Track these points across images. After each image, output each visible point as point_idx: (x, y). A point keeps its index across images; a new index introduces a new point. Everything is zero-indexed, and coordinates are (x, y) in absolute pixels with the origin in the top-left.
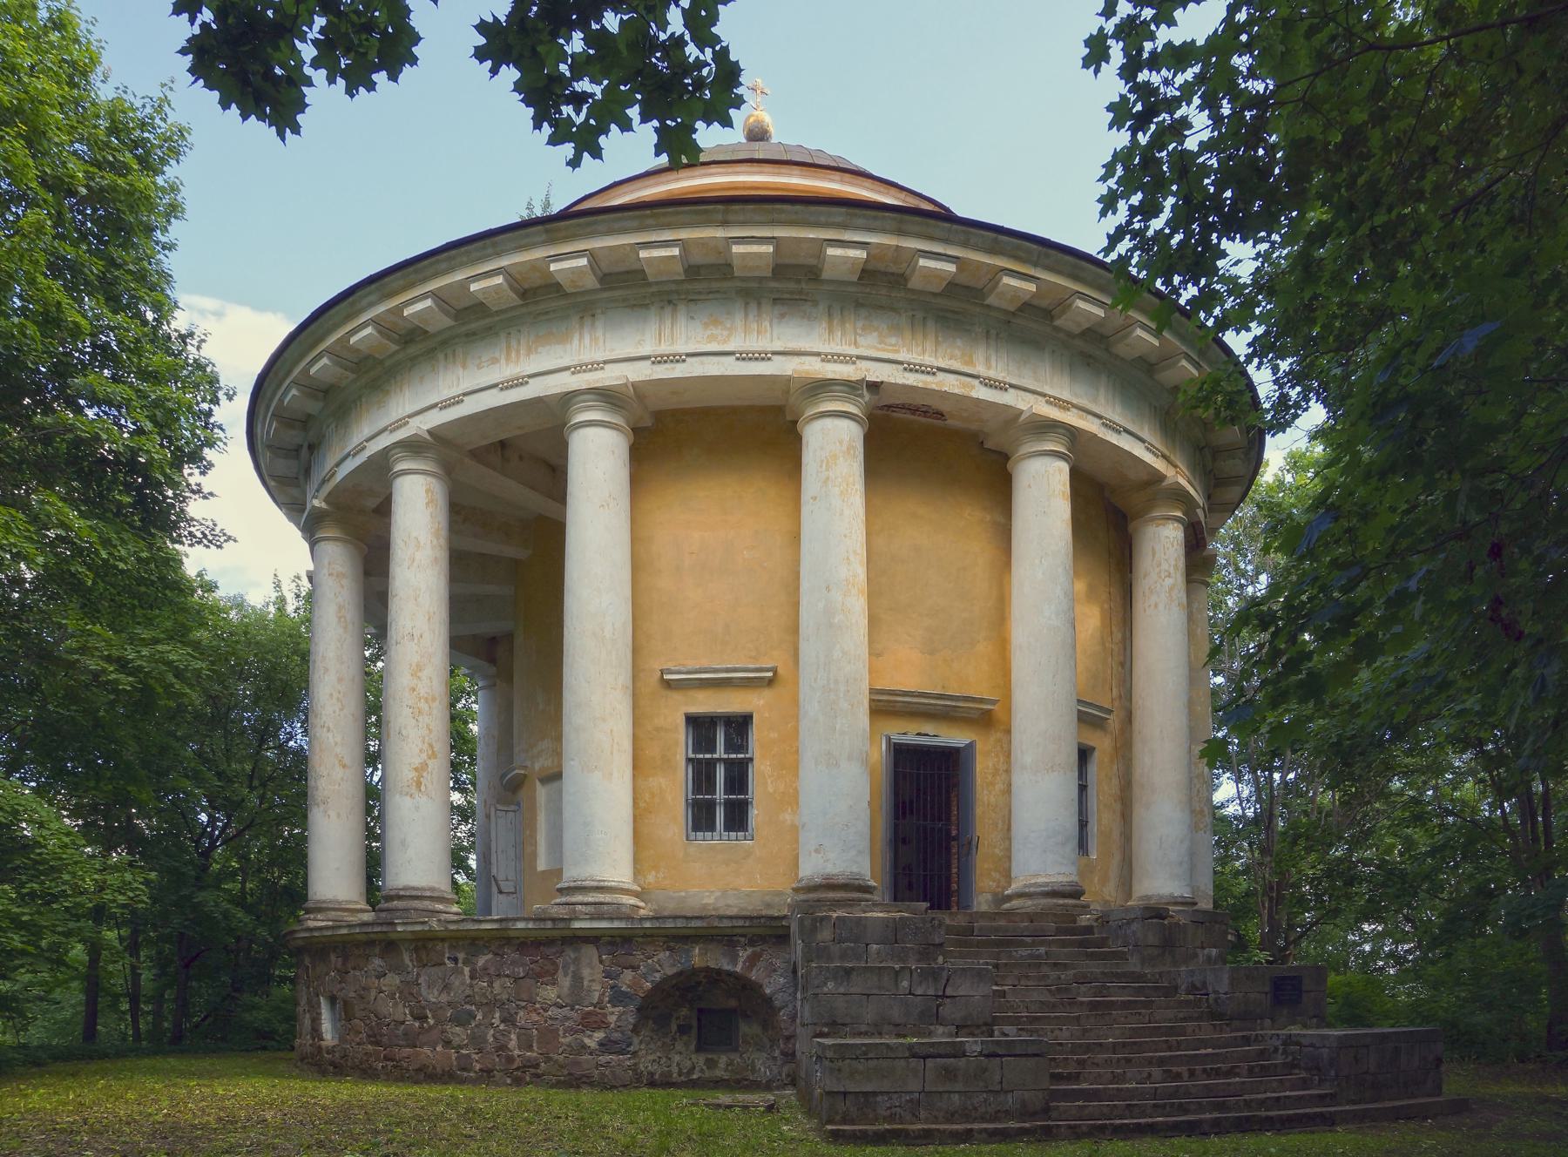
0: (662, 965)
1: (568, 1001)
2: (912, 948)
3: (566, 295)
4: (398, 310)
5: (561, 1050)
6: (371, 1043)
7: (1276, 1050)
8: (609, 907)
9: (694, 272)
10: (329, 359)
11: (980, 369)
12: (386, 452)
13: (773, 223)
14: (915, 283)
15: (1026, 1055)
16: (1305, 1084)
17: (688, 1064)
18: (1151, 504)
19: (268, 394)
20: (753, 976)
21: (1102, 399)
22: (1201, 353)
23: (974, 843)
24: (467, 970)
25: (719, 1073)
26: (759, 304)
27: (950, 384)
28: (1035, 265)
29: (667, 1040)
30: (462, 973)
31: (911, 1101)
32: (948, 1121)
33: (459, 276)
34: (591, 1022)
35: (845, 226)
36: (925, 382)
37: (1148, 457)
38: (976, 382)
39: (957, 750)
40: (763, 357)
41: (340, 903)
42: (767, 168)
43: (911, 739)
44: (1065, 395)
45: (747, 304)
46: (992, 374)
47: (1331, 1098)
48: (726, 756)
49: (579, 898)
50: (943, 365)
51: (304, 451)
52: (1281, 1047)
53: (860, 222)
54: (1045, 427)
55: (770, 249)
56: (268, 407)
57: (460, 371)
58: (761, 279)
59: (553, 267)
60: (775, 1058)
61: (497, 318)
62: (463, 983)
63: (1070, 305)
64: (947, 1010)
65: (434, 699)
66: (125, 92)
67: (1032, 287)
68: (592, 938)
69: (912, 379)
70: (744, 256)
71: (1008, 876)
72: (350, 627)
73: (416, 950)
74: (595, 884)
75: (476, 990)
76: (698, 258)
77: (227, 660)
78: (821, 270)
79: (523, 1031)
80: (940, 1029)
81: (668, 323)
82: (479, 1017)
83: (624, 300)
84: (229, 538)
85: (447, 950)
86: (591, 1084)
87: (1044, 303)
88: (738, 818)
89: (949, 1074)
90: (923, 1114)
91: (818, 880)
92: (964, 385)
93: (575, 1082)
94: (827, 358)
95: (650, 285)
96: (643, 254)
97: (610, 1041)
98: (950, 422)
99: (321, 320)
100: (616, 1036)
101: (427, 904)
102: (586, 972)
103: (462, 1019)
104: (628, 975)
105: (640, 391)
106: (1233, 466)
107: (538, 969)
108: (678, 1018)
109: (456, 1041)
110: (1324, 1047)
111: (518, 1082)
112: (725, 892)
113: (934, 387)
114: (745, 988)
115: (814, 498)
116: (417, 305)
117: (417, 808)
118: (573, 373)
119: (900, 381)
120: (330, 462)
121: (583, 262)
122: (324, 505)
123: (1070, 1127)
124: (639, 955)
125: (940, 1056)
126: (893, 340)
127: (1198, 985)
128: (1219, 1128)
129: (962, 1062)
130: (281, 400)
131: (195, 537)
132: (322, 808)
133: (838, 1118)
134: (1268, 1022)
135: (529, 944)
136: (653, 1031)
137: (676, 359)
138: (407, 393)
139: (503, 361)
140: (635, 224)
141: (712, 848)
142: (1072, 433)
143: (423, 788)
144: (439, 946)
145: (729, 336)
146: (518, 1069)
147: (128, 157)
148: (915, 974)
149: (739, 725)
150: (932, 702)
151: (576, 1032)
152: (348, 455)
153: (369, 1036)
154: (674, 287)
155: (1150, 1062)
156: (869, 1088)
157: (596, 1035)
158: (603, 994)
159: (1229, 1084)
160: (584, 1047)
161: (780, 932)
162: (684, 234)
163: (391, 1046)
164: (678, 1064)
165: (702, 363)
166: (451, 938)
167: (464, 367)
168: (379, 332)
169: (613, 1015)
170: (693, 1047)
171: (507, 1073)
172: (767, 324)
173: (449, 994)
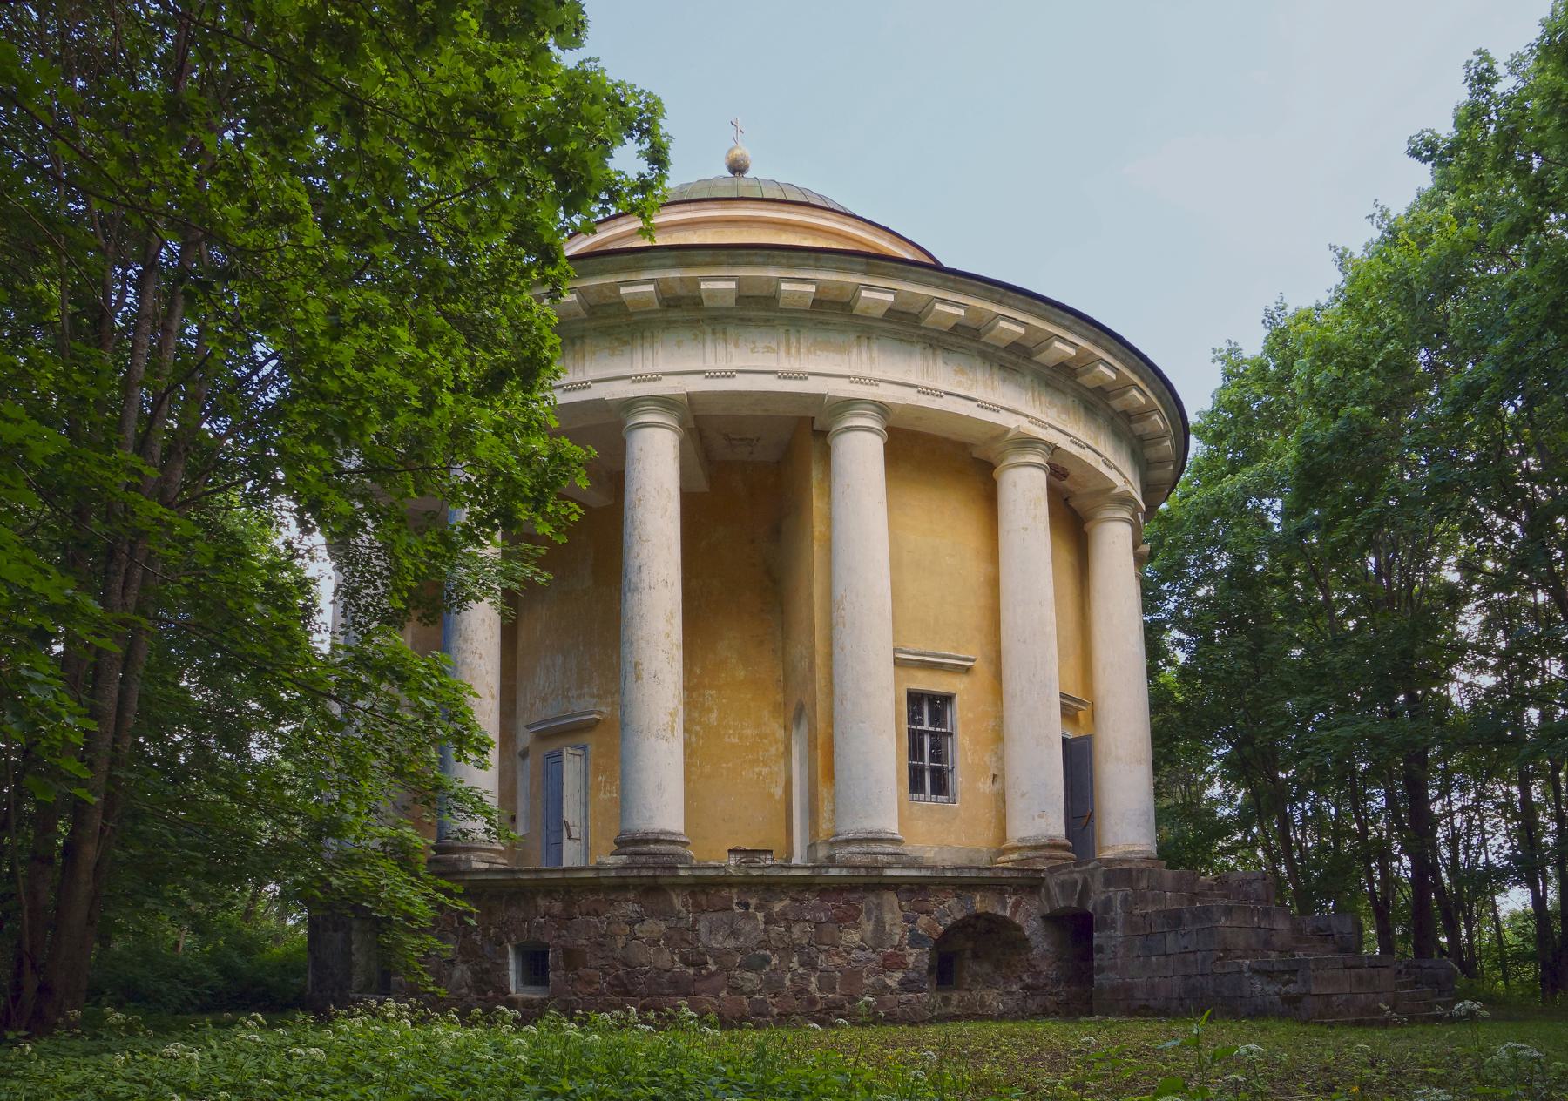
0: (950, 909)
4: (696, 281)
12: (630, 405)
24: (760, 916)
30: (755, 918)
33: (773, 273)
34: (893, 962)
35: (1067, 328)
40: (994, 409)
53: (1078, 329)
55: (733, 285)
57: (731, 348)
58: (997, 348)
60: (1010, 993)
63: (1149, 417)
68: (895, 886)
69: (1074, 450)
70: (790, 293)
73: (693, 894)
82: (775, 961)
85: (735, 896)
88: (940, 787)
92: (1096, 461)
94: (1034, 420)
100: (913, 975)
102: (888, 917)
103: (760, 963)
104: (923, 920)
109: (748, 986)
114: (994, 925)
126: (1064, 417)
137: (937, 394)
140: (939, 282)
146: (819, 1011)
151: (878, 973)
154: (937, 335)
160: (886, 986)
162: (971, 301)
167: (737, 345)
173: (737, 939)
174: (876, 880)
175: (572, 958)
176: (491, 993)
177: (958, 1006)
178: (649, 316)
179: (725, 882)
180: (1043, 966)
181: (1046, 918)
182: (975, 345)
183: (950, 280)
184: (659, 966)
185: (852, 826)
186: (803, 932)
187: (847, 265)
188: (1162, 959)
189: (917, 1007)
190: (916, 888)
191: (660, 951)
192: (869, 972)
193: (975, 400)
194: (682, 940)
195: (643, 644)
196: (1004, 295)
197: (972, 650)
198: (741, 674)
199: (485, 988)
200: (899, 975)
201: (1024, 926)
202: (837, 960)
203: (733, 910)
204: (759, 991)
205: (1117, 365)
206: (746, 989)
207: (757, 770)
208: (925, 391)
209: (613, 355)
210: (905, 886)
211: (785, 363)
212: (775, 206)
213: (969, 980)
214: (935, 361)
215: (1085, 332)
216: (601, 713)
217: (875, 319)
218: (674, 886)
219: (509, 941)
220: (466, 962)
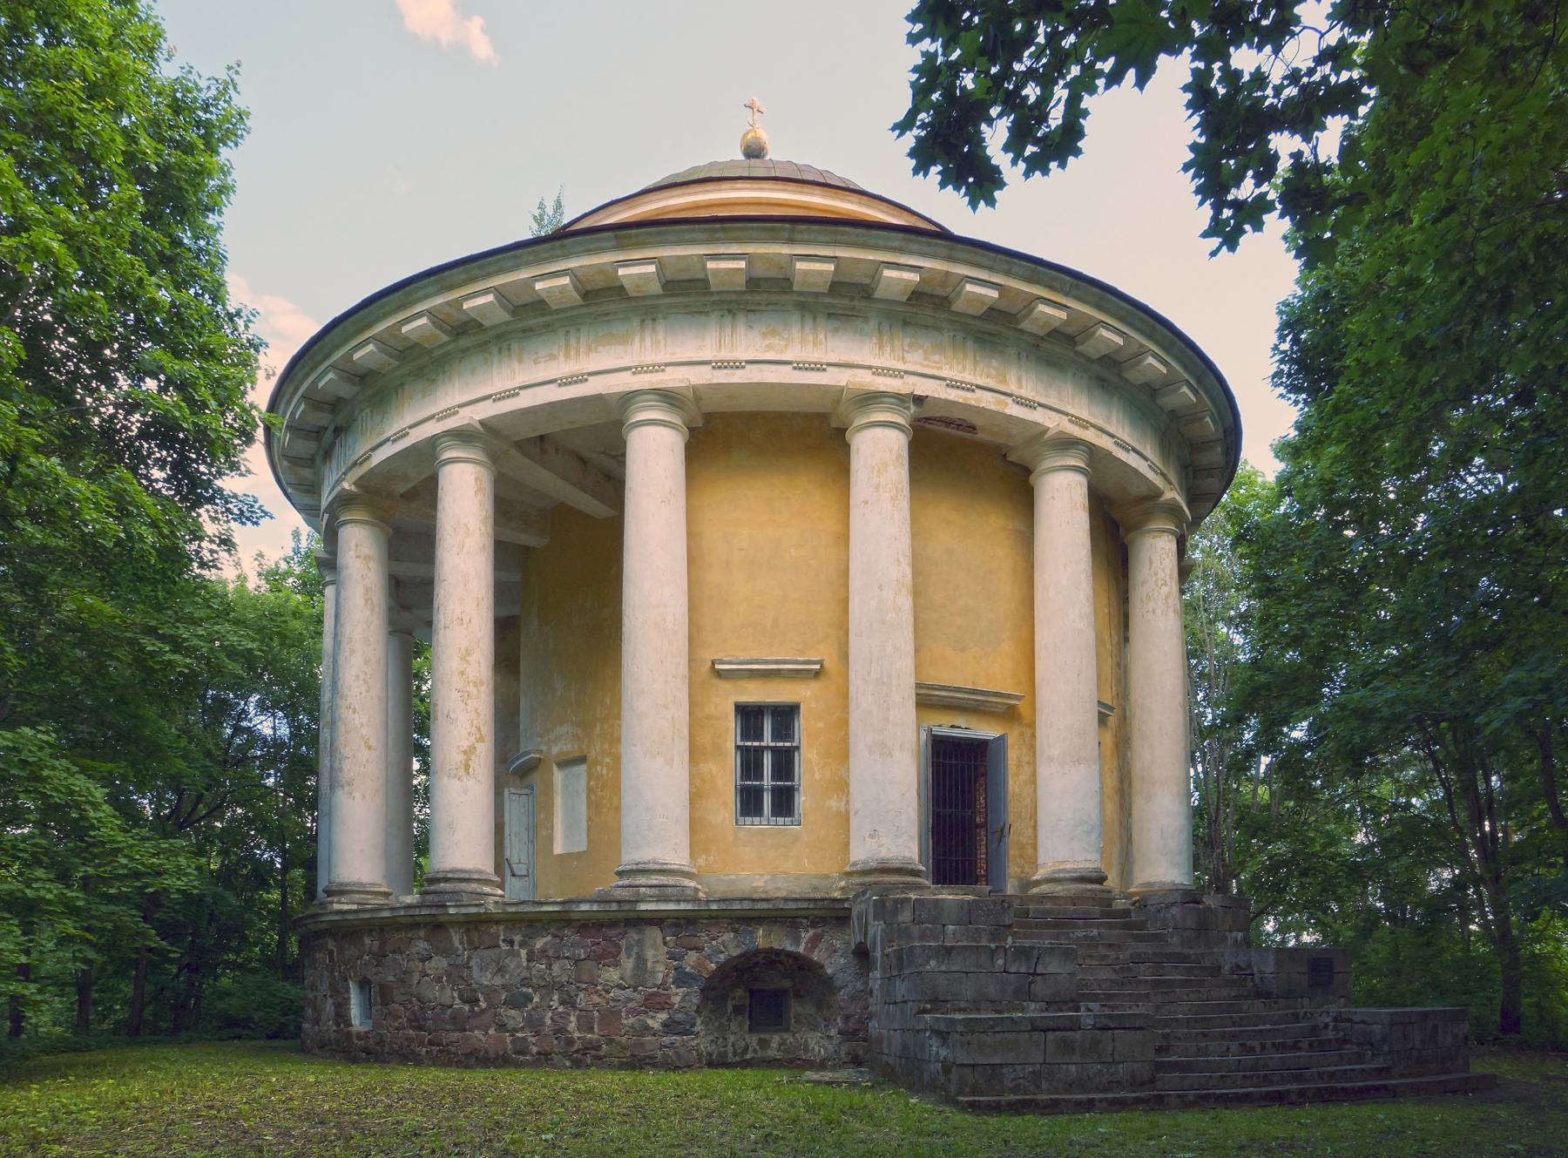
0: (726, 945)
1: (632, 983)
2: (984, 930)
3: (629, 298)
4: (458, 303)
5: (623, 1032)
6: (414, 1028)
7: (1326, 1026)
8: (675, 890)
9: (754, 284)
11: (1012, 388)
12: (433, 443)
13: (836, 243)
14: (959, 306)
16: (1360, 1058)
17: (743, 1044)
18: (1147, 516)
19: (300, 376)
20: (815, 957)
22: (1199, 381)
23: (1007, 829)
24: (523, 952)
25: (772, 1053)
26: (815, 318)
27: (987, 401)
28: (1067, 295)
30: (518, 955)
31: (1033, 1072)
32: (1067, 1091)
33: (524, 274)
34: (655, 1003)
36: (966, 399)
37: (1151, 475)
38: (1009, 400)
40: (818, 367)
41: (362, 884)
42: (792, 186)
43: (945, 731)
44: (1084, 414)
45: (803, 317)
48: (773, 744)
49: (642, 880)
50: (1042, 402)
51: (329, 435)
52: (1332, 1024)
53: (914, 247)
54: (1067, 444)
55: (832, 267)
56: (297, 389)
57: (516, 365)
58: (817, 295)
59: (621, 272)
60: (830, 1038)
63: (1094, 333)
64: (1039, 987)
65: (482, 683)
66: (190, 72)
67: (1063, 315)
68: (656, 920)
70: (806, 272)
71: (1035, 865)
72: (377, 609)
74: (658, 867)
75: (534, 972)
76: (760, 272)
77: (213, 641)
78: (874, 290)
80: (1033, 1006)
81: (728, 331)
82: (536, 999)
83: (686, 307)
84: (266, 513)
86: (655, 1066)
87: (1069, 330)
88: (784, 803)
89: (1067, 1047)
90: (1044, 1085)
91: (873, 864)
92: (1000, 403)
93: (637, 1063)
95: (712, 294)
96: (711, 265)
98: (981, 436)
99: (372, 307)
100: (680, 1016)
101: (474, 886)
102: (650, 954)
103: (518, 1002)
104: (692, 956)
105: (698, 393)
106: (1212, 483)
108: (733, 999)
110: (1376, 1023)
111: (577, 1064)
112: (774, 876)
113: (973, 403)
114: (803, 967)
115: (866, 502)
116: (479, 300)
117: (465, 791)
118: (634, 373)
119: (943, 396)
120: (361, 449)
121: (652, 269)
122: (353, 488)
123: (1179, 1096)
126: (937, 358)
127: (1243, 966)
128: (1302, 1098)
129: (1078, 1035)
130: (315, 383)
131: (232, 513)
132: (347, 789)
133: (967, 1090)
134: (1306, 1001)
135: (588, 925)
136: (711, 1011)
137: (737, 365)
139: (562, 358)
141: (762, 832)
143: (471, 771)
144: (493, 929)
145: (786, 347)
146: (577, 1051)
147: (193, 136)
148: (1009, 953)
149: (785, 716)
150: (966, 696)
151: (638, 1014)
152: (387, 440)
153: (410, 1020)
154: (734, 297)
156: (997, 1060)
157: (659, 1015)
158: (667, 975)
159: (1300, 1057)
160: (647, 1028)
161: (841, 914)
162: (750, 249)
163: (435, 1031)
164: (733, 1045)
165: (761, 371)
167: (520, 361)
168: (434, 323)
169: (677, 996)
170: (746, 1027)
171: (566, 1055)
172: (822, 336)
173: (503, 976)
182: (788, 297)
183: (716, 230)
184: (442, 1002)
185: (632, 855)
186: (563, 969)
189: (682, 1051)
191: (443, 988)
192: (628, 1013)
196: (793, 231)
200: (663, 1016)
201: (826, 963)
202: (596, 999)
203: (499, 946)
204: (522, 1029)
205: (995, 279)
206: (509, 1027)
208: (720, 365)
209: (424, 396)
211: (563, 367)
212: (679, 191)
215: (926, 249)
216: (541, 752)
217: (657, 297)
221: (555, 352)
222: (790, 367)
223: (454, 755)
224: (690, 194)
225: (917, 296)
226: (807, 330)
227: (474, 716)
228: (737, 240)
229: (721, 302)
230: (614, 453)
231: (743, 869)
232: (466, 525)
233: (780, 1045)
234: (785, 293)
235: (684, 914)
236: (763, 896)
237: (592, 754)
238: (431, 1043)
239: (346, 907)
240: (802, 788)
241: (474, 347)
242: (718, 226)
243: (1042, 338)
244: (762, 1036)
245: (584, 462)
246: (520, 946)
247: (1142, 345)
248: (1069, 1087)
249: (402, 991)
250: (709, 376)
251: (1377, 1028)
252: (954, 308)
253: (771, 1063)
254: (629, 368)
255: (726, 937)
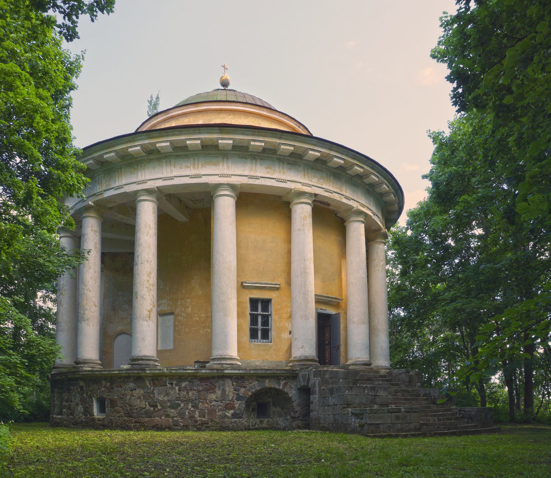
0: (255, 386)
1: (220, 399)
4: (155, 144)
5: (217, 417)
6: (127, 416)
7: (456, 413)
9: (264, 150)
10: (115, 154)
11: (344, 193)
13: (295, 141)
14: (330, 164)
15: (416, 412)
16: (468, 423)
17: (254, 422)
21: (372, 205)
24: (177, 388)
25: (264, 425)
26: (283, 164)
27: (336, 197)
28: (364, 163)
29: (249, 413)
30: (175, 389)
31: (388, 426)
33: (183, 137)
34: (229, 407)
35: (315, 145)
37: (380, 223)
39: (331, 315)
40: (284, 181)
46: (347, 195)
47: (475, 426)
48: (262, 313)
50: (335, 191)
53: (320, 144)
54: (360, 213)
57: (173, 168)
58: (285, 156)
60: (287, 420)
61: (190, 153)
62: (175, 393)
64: (378, 400)
67: (362, 170)
68: (230, 377)
69: (327, 194)
73: (153, 380)
76: (268, 146)
79: (201, 411)
81: (254, 165)
82: (182, 405)
83: (239, 155)
88: (266, 335)
89: (398, 418)
90: (391, 430)
91: (303, 358)
92: (340, 198)
93: (223, 428)
94: (304, 184)
97: (236, 414)
98: (331, 207)
100: (238, 412)
101: (152, 362)
102: (227, 389)
103: (175, 406)
104: (243, 390)
107: (208, 388)
109: (172, 415)
112: (263, 361)
113: (332, 197)
114: (279, 393)
115: (299, 230)
117: (149, 326)
118: (220, 177)
122: (93, 204)
124: (247, 382)
125: (395, 412)
126: (321, 181)
129: (400, 414)
132: (86, 322)
133: (370, 432)
137: (257, 178)
138: (147, 171)
139: (192, 168)
140: (251, 133)
142: (366, 215)
143: (151, 318)
144: (164, 379)
145: (273, 173)
146: (199, 425)
149: (266, 303)
151: (223, 410)
154: (256, 154)
155: (434, 416)
156: (378, 422)
160: (226, 416)
162: (267, 139)
166: (170, 376)
167: (175, 167)
168: (142, 149)
169: (237, 404)
171: (195, 426)
173: (168, 397)
174: (221, 374)
175: (113, 403)
176: (88, 416)
177: (267, 424)
178: (143, 158)
179: (164, 375)
180: (297, 409)
181: (298, 389)
183: (256, 132)
184: (141, 406)
185: (216, 353)
187: (211, 131)
188: (328, 407)
189: (239, 424)
190: (239, 377)
191: (141, 401)
192: (219, 410)
193: (275, 179)
194: (149, 397)
195: (139, 285)
197: (281, 281)
198: (200, 292)
199: (87, 414)
200: (232, 412)
202: (206, 405)
204: (176, 417)
207: (206, 330)
209: (131, 174)
210: (235, 377)
213: (272, 414)
214: (256, 164)
217: (229, 150)
218: (146, 376)
219: (94, 397)
220: (82, 404)
221: (189, 165)
222: (275, 180)
223: (145, 312)
224: (219, 105)
225: (318, 160)
226: (281, 168)
227: (152, 297)
228: (262, 136)
229: (251, 155)
230: (193, 199)
231: (252, 359)
232: (149, 225)
233: (268, 422)
234: (274, 154)
235: (240, 374)
236: (259, 368)
237: (177, 312)
238: (136, 422)
239: (88, 369)
240: (273, 330)
241: (155, 159)
242: (256, 130)
243: (353, 176)
244: (261, 419)
245: (180, 201)
246: (176, 385)
247: (383, 181)
248: (398, 431)
249: (122, 402)
250: (247, 181)
251: (473, 413)
252: (328, 165)
253: (264, 429)
254: (218, 175)
255: (255, 383)
